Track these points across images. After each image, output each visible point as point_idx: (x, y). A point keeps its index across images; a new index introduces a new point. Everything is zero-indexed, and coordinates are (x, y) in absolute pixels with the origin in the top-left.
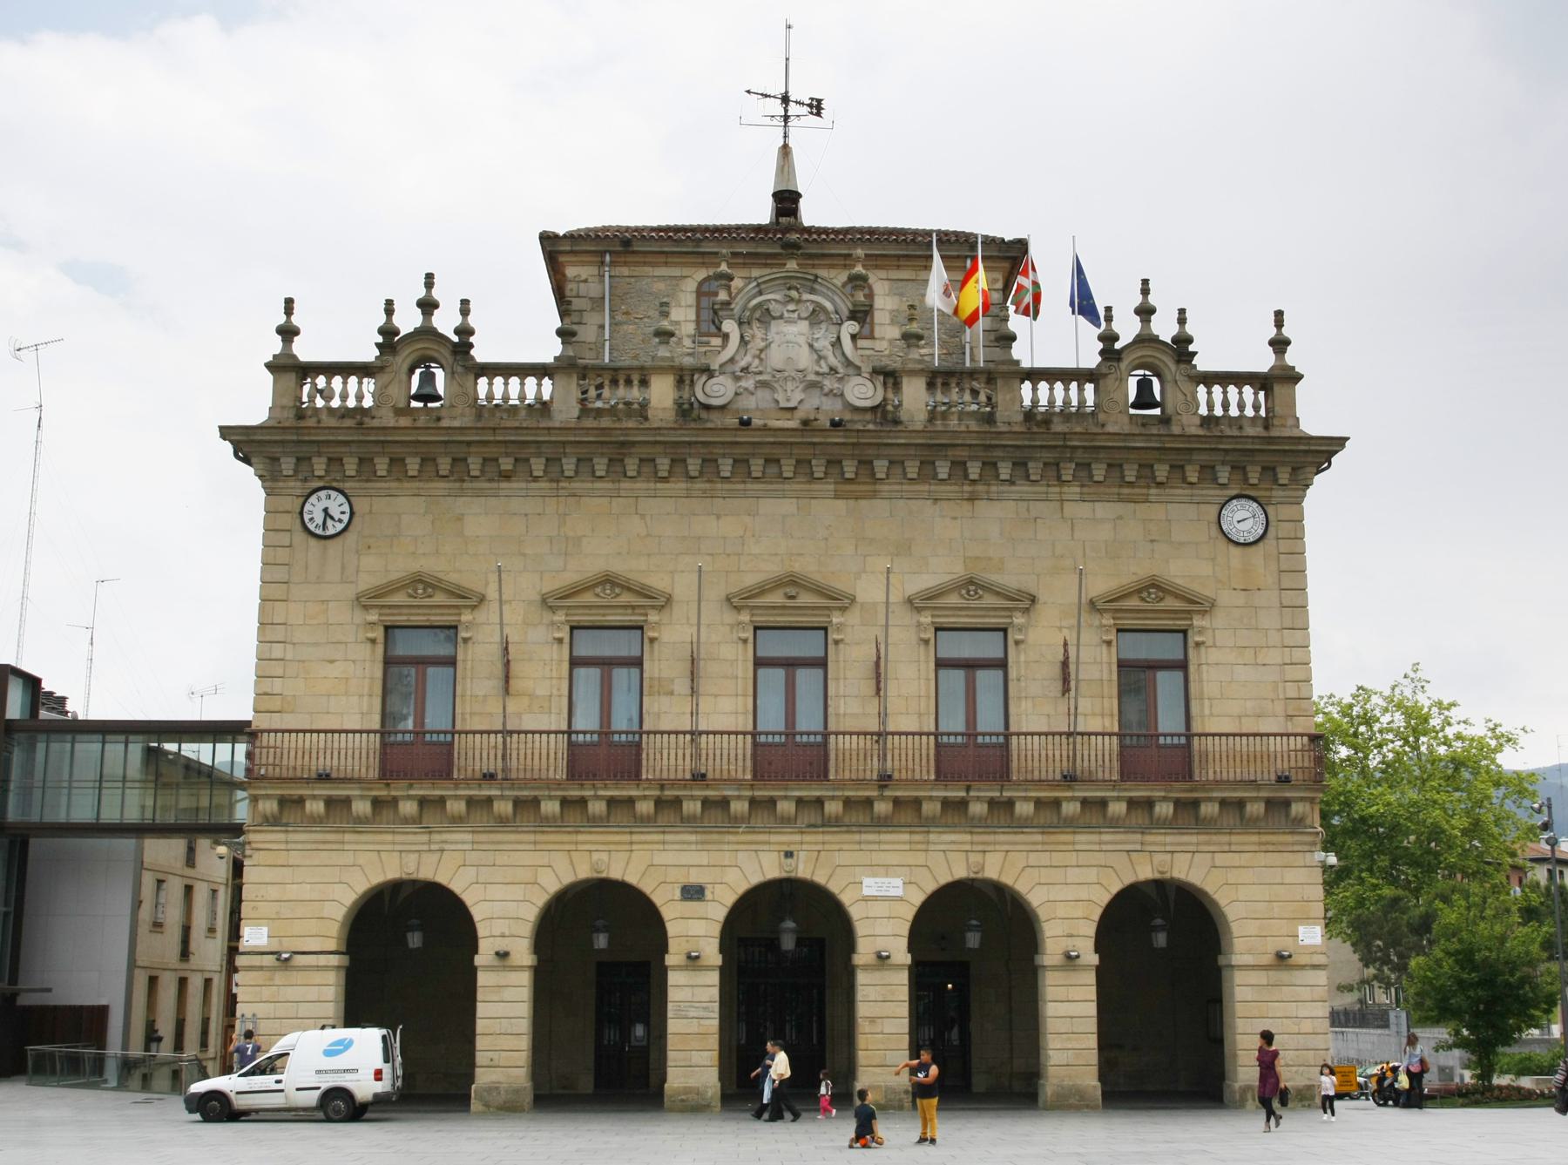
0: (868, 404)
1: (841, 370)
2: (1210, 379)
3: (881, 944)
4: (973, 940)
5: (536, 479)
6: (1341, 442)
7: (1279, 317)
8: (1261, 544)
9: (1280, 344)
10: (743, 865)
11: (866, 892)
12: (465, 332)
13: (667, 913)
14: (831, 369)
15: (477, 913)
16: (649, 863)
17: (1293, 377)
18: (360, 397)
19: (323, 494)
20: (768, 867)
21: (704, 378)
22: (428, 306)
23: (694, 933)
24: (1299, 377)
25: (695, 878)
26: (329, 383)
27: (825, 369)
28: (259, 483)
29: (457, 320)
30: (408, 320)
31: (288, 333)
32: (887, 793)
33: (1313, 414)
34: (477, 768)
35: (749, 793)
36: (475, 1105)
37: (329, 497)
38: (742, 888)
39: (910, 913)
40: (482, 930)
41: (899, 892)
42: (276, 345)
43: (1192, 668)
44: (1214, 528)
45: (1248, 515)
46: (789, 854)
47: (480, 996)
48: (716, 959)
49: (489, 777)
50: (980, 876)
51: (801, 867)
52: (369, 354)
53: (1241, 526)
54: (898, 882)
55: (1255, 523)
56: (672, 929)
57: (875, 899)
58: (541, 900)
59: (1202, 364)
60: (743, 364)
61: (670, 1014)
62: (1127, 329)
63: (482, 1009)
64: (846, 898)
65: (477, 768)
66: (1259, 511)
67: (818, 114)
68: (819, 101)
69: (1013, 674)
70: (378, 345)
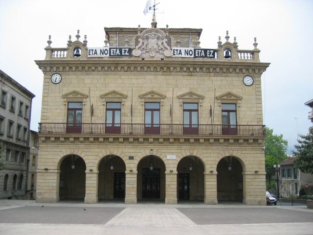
2: (241, 52)
4: (191, 169)
6: (270, 64)
9: (255, 45)
12: (85, 42)
13: (126, 162)
15: (86, 162)
16: (122, 151)
18: (64, 55)
20: (147, 153)
22: (78, 37)
23: (132, 167)
25: (131, 155)
29: (84, 39)
30: (74, 39)
31: (49, 42)
33: (262, 59)
39: (177, 163)
41: (175, 158)
42: (47, 45)
43: (237, 112)
44: (242, 82)
47: (86, 179)
52: (66, 46)
57: (170, 160)
59: (240, 48)
64: (164, 159)
66: (252, 79)
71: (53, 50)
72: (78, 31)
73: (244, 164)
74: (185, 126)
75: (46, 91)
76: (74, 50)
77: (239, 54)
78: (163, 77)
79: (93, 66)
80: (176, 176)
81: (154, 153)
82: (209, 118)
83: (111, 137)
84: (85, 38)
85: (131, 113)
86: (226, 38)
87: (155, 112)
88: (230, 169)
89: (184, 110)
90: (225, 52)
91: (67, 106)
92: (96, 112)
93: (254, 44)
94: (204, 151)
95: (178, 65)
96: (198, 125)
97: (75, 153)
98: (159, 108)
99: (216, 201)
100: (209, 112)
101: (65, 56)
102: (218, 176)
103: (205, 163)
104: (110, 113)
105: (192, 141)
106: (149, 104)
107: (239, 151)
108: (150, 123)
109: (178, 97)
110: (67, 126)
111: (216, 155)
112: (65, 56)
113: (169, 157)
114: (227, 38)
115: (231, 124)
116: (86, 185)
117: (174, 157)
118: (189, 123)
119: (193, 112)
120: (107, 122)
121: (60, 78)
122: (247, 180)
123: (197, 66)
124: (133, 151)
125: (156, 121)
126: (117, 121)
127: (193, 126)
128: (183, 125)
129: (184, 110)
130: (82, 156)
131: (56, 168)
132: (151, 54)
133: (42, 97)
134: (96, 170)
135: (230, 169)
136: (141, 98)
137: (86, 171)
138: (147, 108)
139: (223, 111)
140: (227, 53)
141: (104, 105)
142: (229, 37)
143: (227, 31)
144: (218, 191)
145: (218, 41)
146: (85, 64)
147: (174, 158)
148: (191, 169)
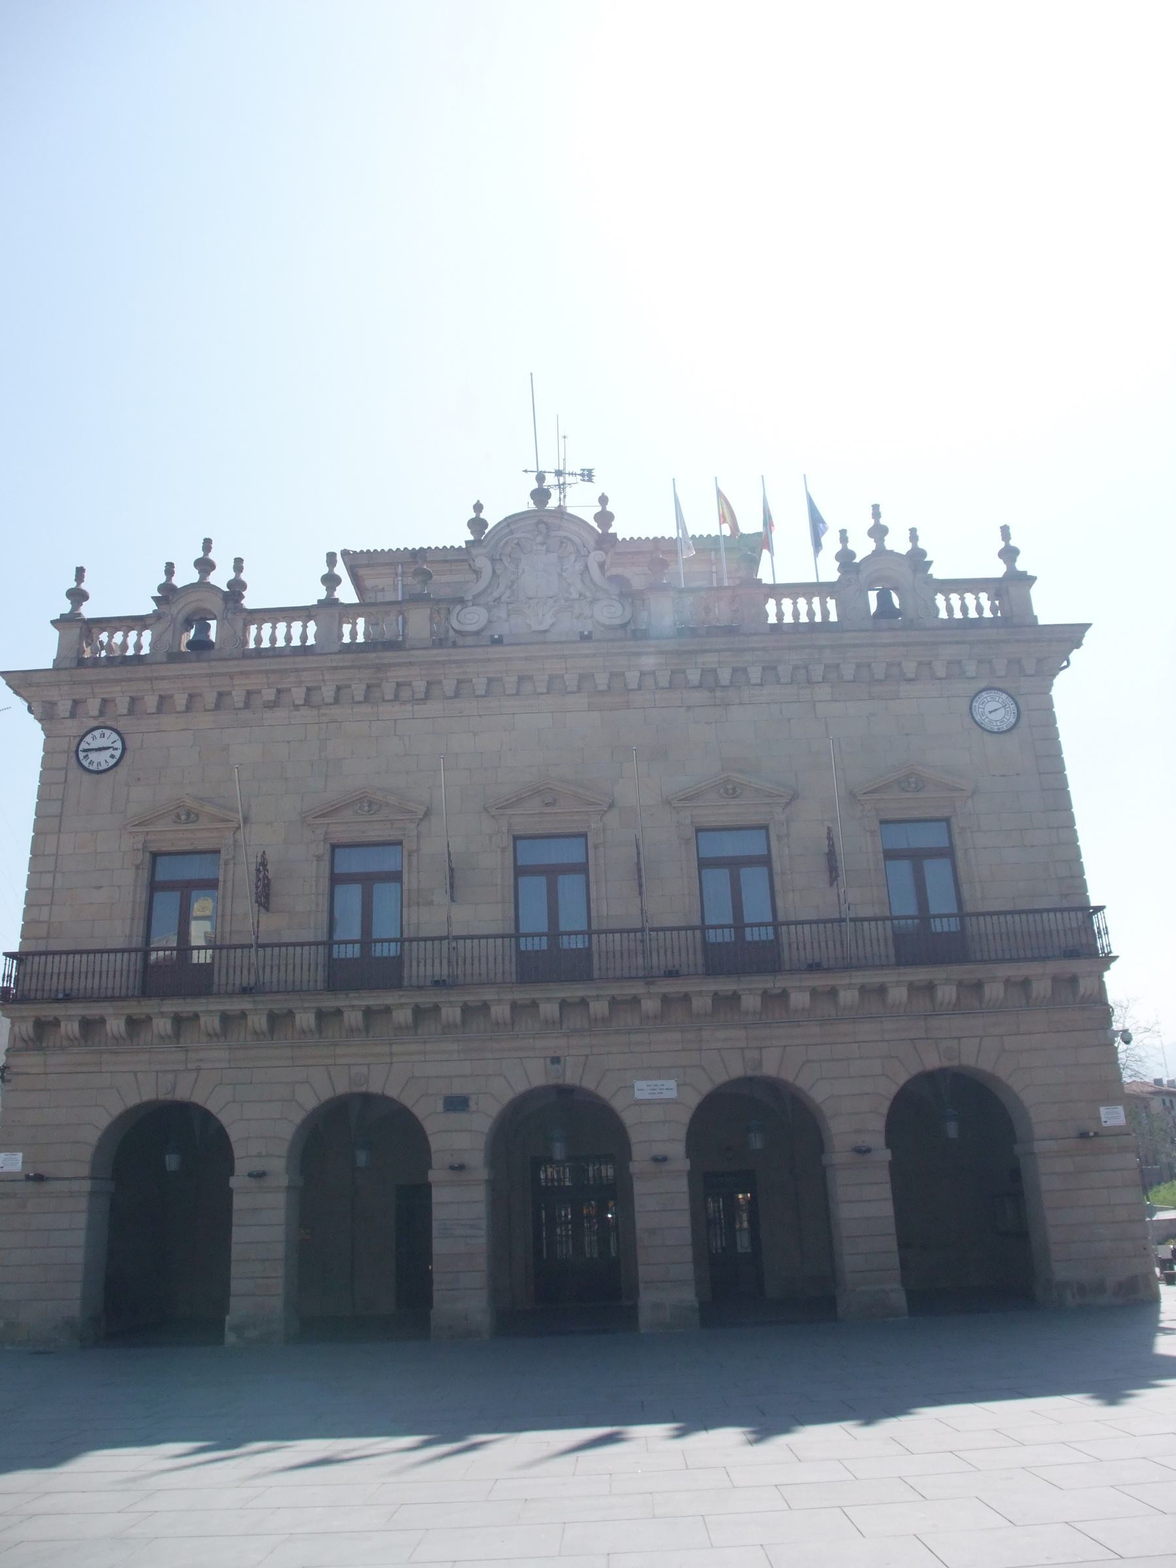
0: (618, 622)
1: (588, 594)
3: (659, 1149)
4: (757, 1142)
5: (297, 707)
7: (80, 573)
9: (1009, 554)
10: (509, 1070)
11: (638, 1095)
13: (430, 1126)
14: (580, 594)
15: (234, 1134)
16: (413, 1069)
17: (1027, 580)
18: (304, 637)
19: (97, 733)
21: (459, 607)
22: (205, 565)
23: (459, 1144)
24: (1033, 579)
25: (458, 1089)
26: (111, 637)
27: (575, 595)
28: (39, 726)
29: (232, 575)
30: (186, 576)
31: (78, 596)
32: (654, 989)
34: (237, 982)
35: (510, 997)
36: (230, 1338)
37: (103, 735)
38: (508, 1096)
39: (685, 1117)
40: (237, 1152)
41: (672, 1094)
42: (66, 607)
43: (959, 854)
45: (999, 705)
46: (556, 1060)
47: (236, 1219)
48: (483, 1174)
49: (438, 984)
50: (757, 1073)
52: (149, 608)
53: (993, 716)
54: (672, 1084)
55: (1007, 712)
56: (435, 1143)
57: (648, 1103)
58: (298, 1117)
59: (938, 572)
60: (496, 595)
61: (435, 1233)
62: (863, 547)
63: (238, 1235)
64: (617, 1104)
65: (237, 982)
66: (1010, 702)
67: (590, 480)
68: (590, 471)
69: (777, 867)
70: (154, 598)
72: (207, 545)
74: (712, 936)
76: (188, 624)
80: (683, 1185)
83: (353, 1006)
85: (452, 887)
86: (871, 533)
88: (952, 1130)
90: (872, 597)
91: (325, 865)
98: (945, 843)
99: (899, 1298)
101: (145, 651)
102: (896, 1169)
104: (719, 880)
105: (751, 1002)
108: (729, 920)
112: (311, 641)
113: (643, 1089)
115: (934, 909)
116: (236, 1251)
117: (668, 1089)
118: (729, 920)
119: (561, 879)
126: (384, 927)
128: (704, 928)
131: (85, 1170)
135: (952, 1130)
137: (233, 1182)
138: (524, 860)
139: (890, 855)
145: (163, 579)
146: (231, 676)
148: (757, 1142)
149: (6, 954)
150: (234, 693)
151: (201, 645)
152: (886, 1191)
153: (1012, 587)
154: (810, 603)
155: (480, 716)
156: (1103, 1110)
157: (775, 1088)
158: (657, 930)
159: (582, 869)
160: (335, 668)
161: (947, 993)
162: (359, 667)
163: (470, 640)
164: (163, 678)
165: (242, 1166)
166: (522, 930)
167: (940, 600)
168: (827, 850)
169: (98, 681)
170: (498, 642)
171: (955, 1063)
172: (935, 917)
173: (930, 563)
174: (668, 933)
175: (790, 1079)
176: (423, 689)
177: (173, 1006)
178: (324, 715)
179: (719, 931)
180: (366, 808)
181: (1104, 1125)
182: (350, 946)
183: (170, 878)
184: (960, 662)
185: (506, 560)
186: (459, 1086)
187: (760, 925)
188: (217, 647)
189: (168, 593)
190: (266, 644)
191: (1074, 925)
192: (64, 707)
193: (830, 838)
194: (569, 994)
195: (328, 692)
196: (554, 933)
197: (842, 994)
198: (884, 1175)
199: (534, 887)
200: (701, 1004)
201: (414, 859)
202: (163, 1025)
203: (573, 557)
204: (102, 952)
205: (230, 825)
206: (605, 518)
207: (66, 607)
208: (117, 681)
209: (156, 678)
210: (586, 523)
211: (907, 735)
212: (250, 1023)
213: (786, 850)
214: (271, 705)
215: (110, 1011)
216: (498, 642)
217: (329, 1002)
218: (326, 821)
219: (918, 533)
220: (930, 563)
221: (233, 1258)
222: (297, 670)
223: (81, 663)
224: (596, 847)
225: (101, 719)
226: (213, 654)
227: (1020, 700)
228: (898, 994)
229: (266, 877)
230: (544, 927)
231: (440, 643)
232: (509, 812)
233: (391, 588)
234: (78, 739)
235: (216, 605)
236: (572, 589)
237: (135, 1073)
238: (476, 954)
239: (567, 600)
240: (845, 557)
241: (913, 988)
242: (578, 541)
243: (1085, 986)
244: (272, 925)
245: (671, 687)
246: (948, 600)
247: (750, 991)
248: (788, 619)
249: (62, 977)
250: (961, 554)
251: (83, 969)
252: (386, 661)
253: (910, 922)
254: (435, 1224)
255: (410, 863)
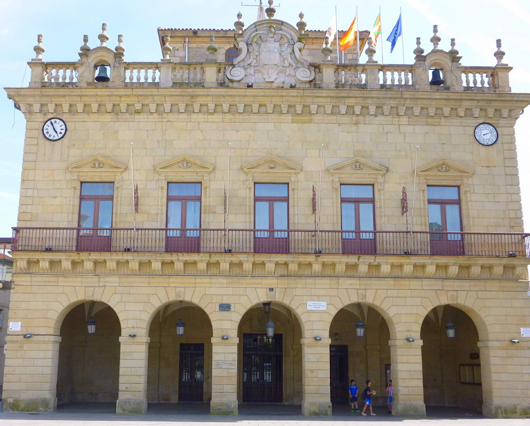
1: (294, 65)
5: (152, 113)
8: (495, 145)
9: (499, 55)
11: (309, 308)
13: (212, 317)
14: (290, 64)
21: (231, 68)
25: (225, 301)
26: (57, 72)
27: (287, 65)
36: (118, 410)
38: (249, 306)
39: (330, 319)
40: (123, 325)
41: (325, 308)
42: (33, 55)
43: (463, 204)
46: (271, 290)
47: (121, 357)
51: (277, 296)
52: (76, 58)
53: (485, 137)
54: (324, 303)
55: (492, 136)
56: (214, 325)
57: (312, 312)
59: (464, 63)
60: (249, 62)
61: (213, 367)
62: (427, 48)
64: (299, 311)
69: (377, 204)
71: (47, 66)
73: (484, 322)
74: (259, 234)
75: (32, 157)
76: (96, 67)
77: (463, 76)
78: (295, 125)
79: (139, 102)
81: (278, 297)
82: (227, 213)
84: (120, 41)
86: (432, 40)
87: (276, 204)
89: (343, 200)
90: (430, 72)
92: (146, 204)
93: (495, 55)
94: (390, 293)
95: (329, 100)
96: (288, 231)
97: (97, 298)
99: (175, 398)
100: (399, 203)
103: (395, 320)
106: (95, 184)
107: (470, 293)
108: (179, 227)
109: (327, 170)
110: (78, 233)
111: (418, 301)
113: (311, 305)
114: (436, 40)
116: (122, 371)
117: (322, 306)
118: (179, 227)
120: (169, 226)
121: (64, 127)
122: (494, 361)
123: (370, 101)
124: (230, 291)
125: (280, 224)
127: (276, 235)
128: (254, 231)
129: (343, 200)
130: (111, 304)
131: (51, 331)
132: (266, 77)
133: (21, 169)
134: (143, 337)
136: (333, 175)
137: (121, 339)
138: (173, 193)
140: (436, 74)
141: (162, 188)
142: (439, 39)
143: (120, 36)
144: (425, 386)
145: (415, 47)
146: (121, 96)
147: (322, 308)
149: (12, 228)
150: (121, 105)
151: (102, 79)
152: (420, 359)
153: (497, 72)
154: (400, 75)
155: (240, 122)
156: (522, 329)
157: (448, 308)
158: (322, 231)
159: (286, 199)
160: (172, 96)
161: (454, 270)
162: (182, 96)
163: (235, 85)
164: (86, 96)
165: (125, 332)
166: (256, 228)
167: (463, 76)
168: (401, 197)
169: (54, 95)
170: (250, 86)
171: (455, 302)
172: (363, 232)
173: (460, 58)
174: (327, 233)
175: (378, 304)
176: (213, 108)
177: (95, 256)
178: (165, 118)
179: (367, 234)
180: (185, 165)
181: (522, 336)
182: (175, 231)
183: (95, 194)
184: (471, 109)
185: (254, 44)
186: (226, 300)
187: (281, 231)
188: (111, 80)
189: (85, 51)
190: (135, 80)
191: (513, 241)
192: (36, 107)
193: (404, 192)
194: (280, 260)
195: (167, 107)
196: (183, 230)
197: (405, 266)
198: (419, 352)
199: (263, 207)
200: (340, 268)
201: (208, 190)
202: (89, 265)
203: (286, 45)
204: (57, 229)
205: (120, 170)
206: (301, 25)
207: (33, 55)
208: (64, 96)
209: (83, 95)
210: (291, 26)
211: (443, 144)
212: (85, 265)
213: (382, 197)
214: (138, 112)
215: (64, 257)
216: (250, 86)
217: (168, 257)
218: (166, 170)
219: (455, 41)
220: (460, 58)
221: (120, 374)
222: (152, 95)
223: (44, 85)
224: (293, 190)
225: (55, 114)
226: (109, 84)
227: (498, 129)
228: (431, 269)
229: (137, 196)
230: (353, 228)
231: (222, 85)
232: (253, 170)
233: (182, 52)
234: (43, 124)
235: (110, 59)
236: (286, 61)
237: (75, 286)
238: (61, 237)
239: (283, 67)
240: (419, 52)
241: (438, 266)
242: (288, 36)
243: (518, 270)
244: (142, 220)
245: (332, 113)
246: (467, 77)
247: (364, 263)
248: (389, 82)
249: (37, 240)
250: (476, 53)
251: (48, 236)
252: (196, 93)
253: (88, 232)
254: (213, 363)
255: (205, 193)
